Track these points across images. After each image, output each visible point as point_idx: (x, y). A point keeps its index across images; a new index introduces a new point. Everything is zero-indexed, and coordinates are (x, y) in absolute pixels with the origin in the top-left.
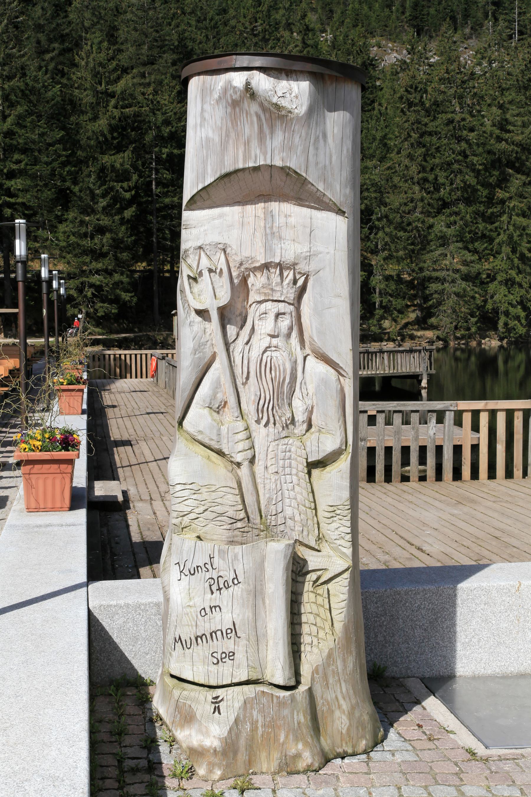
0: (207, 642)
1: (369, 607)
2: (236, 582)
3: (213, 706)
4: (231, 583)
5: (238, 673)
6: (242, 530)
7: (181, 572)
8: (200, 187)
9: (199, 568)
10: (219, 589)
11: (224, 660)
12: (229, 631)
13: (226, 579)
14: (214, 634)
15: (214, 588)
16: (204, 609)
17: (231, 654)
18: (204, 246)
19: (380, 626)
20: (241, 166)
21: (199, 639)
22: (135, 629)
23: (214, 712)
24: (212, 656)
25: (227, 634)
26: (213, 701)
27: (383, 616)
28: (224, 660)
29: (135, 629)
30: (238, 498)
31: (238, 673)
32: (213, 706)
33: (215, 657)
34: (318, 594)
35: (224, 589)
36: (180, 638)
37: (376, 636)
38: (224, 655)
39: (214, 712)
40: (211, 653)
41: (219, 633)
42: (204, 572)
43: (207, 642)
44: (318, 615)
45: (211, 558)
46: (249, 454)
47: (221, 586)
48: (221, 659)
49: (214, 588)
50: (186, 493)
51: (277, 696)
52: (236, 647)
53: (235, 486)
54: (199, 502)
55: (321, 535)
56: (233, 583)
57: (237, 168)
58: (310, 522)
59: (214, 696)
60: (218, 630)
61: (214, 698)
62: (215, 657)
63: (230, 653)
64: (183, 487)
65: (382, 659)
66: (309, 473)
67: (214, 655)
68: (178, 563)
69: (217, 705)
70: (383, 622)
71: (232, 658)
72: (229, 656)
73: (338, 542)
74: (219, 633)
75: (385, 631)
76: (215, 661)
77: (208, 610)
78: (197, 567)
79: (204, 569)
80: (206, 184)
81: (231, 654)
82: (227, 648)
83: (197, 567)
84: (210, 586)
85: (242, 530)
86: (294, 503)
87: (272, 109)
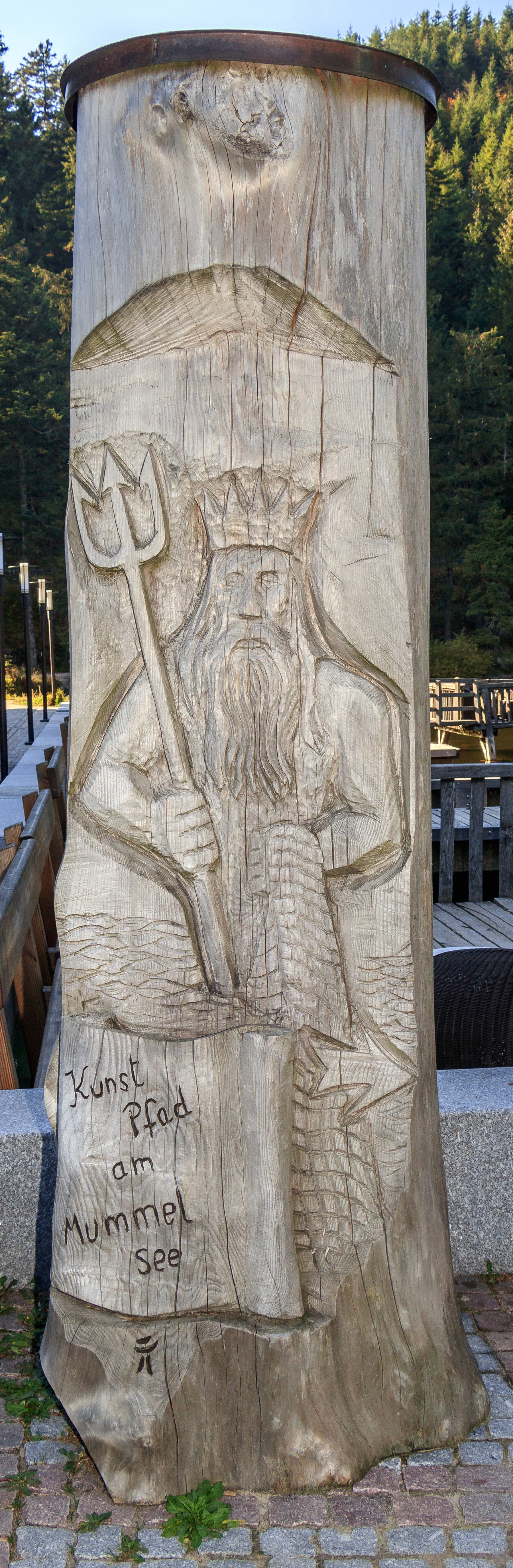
0: (127, 1230)
1: (473, 1143)
2: (182, 1112)
3: (138, 1356)
4: (171, 1114)
5: (188, 1294)
6: (197, 1007)
7: (77, 1090)
8: (98, 320)
9: (111, 1083)
10: (150, 1125)
11: (160, 1266)
12: (169, 1209)
13: (161, 1105)
14: (139, 1214)
15: (140, 1123)
16: (120, 1164)
17: (173, 1255)
18: (111, 441)
19: (496, 1179)
20: (174, 271)
21: (112, 1225)
22: (30, 1185)
23: (140, 1369)
24: (138, 1257)
25: (165, 1214)
26: (138, 1346)
27: (500, 1160)
28: (160, 1266)
29: (30, 1185)
30: (188, 945)
31: (188, 1294)
32: (138, 1356)
33: (142, 1260)
34: (351, 1134)
35: (159, 1125)
36: (75, 1221)
37: (489, 1198)
38: (160, 1257)
39: (140, 1369)
40: (135, 1250)
41: (149, 1212)
42: (119, 1090)
43: (127, 1230)
44: (351, 1176)
45: (132, 1064)
46: (209, 856)
47: (154, 1118)
48: (155, 1264)
49: (140, 1123)
50: (88, 934)
51: (264, 1340)
52: (184, 1242)
53: (180, 918)
54: (112, 952)
55: (354, 1017)
56: (176, 1113)
57: (166, 275)
58: (331, 992)
59: (140, 1337)
60: (149, 1206)
61: (141, 1341)
62: (142, 1260)
63: (171, 1251)
64: (81, 922)
65: (499, 1241)
66: (328, 895)
67: (141, 1254)
68: (71, 1072)
69: (145, 1355)
70: (502, 1172)
71: (174, 1262)
72: (170, 1259)
73: (390, 1031)
74: (149, 1212)
75: (505, 1189)
76: (143, 1267)
77: (128, 1166)
78: (107, 1081)
79: (119, 1085)
80: (109, 314)
81: (173, 1255)
82: (166, 1244)
83: (107, 1081)
84: (132, 1118)
85: (197, 1007)
86: (299, 953)
87: (230, 147)
